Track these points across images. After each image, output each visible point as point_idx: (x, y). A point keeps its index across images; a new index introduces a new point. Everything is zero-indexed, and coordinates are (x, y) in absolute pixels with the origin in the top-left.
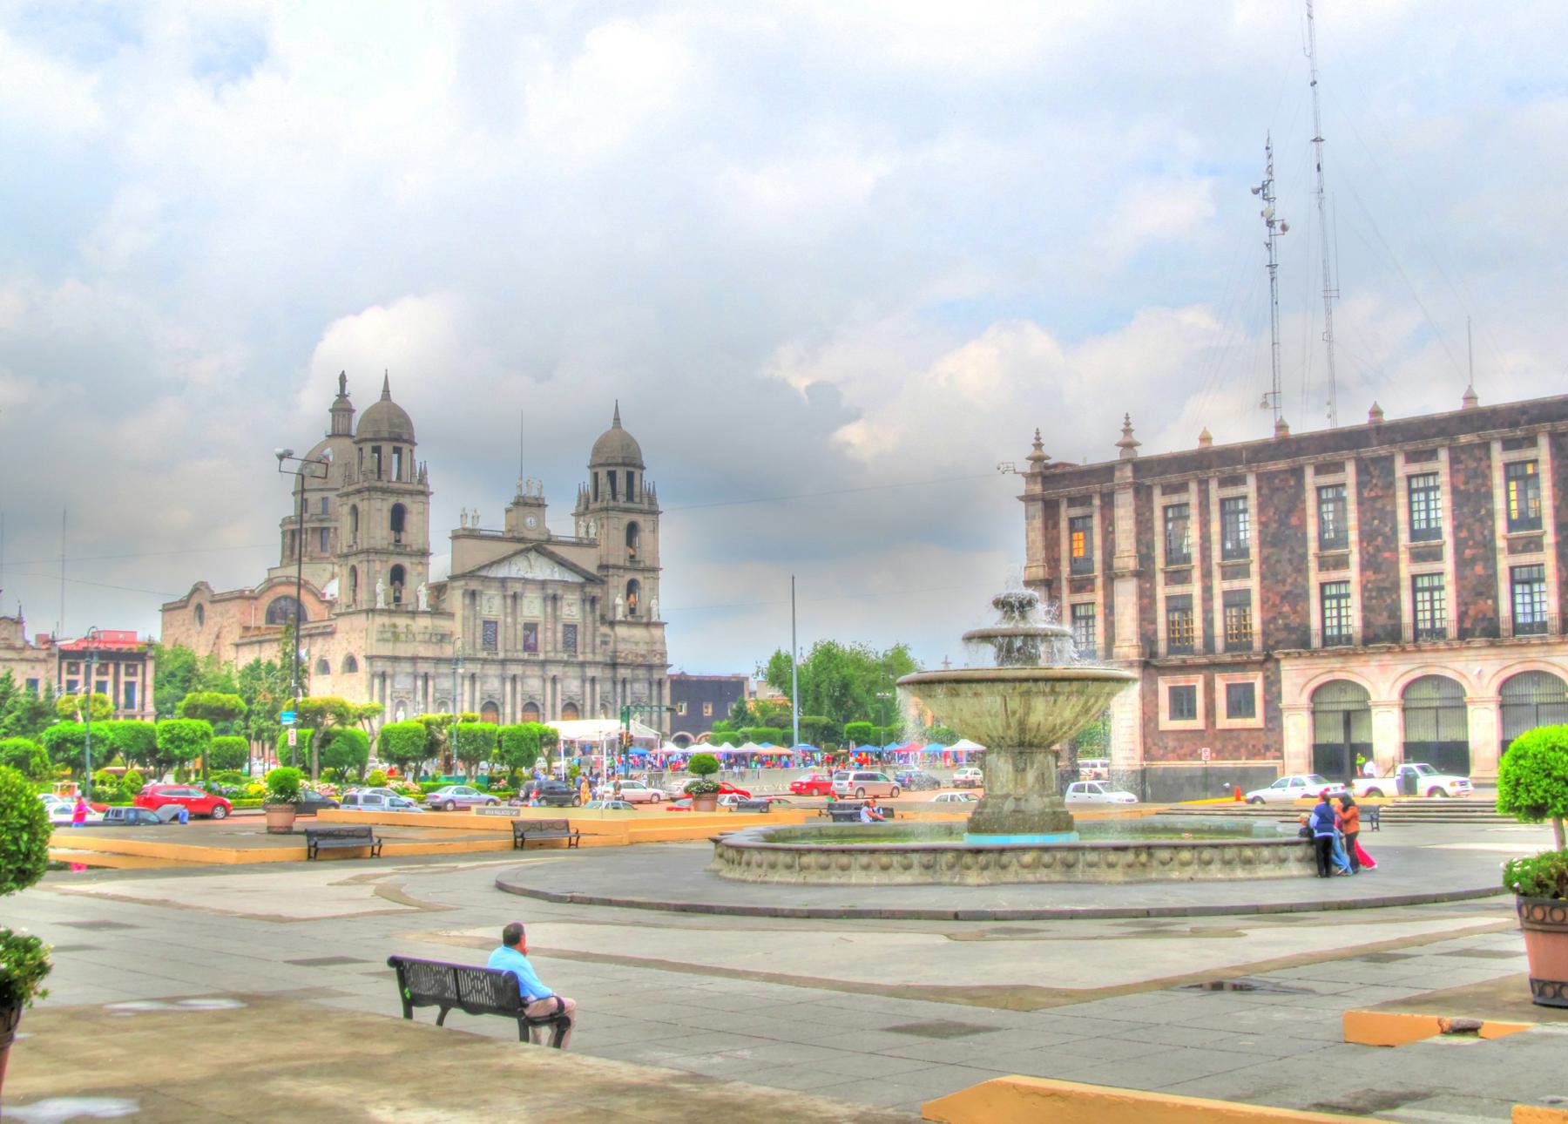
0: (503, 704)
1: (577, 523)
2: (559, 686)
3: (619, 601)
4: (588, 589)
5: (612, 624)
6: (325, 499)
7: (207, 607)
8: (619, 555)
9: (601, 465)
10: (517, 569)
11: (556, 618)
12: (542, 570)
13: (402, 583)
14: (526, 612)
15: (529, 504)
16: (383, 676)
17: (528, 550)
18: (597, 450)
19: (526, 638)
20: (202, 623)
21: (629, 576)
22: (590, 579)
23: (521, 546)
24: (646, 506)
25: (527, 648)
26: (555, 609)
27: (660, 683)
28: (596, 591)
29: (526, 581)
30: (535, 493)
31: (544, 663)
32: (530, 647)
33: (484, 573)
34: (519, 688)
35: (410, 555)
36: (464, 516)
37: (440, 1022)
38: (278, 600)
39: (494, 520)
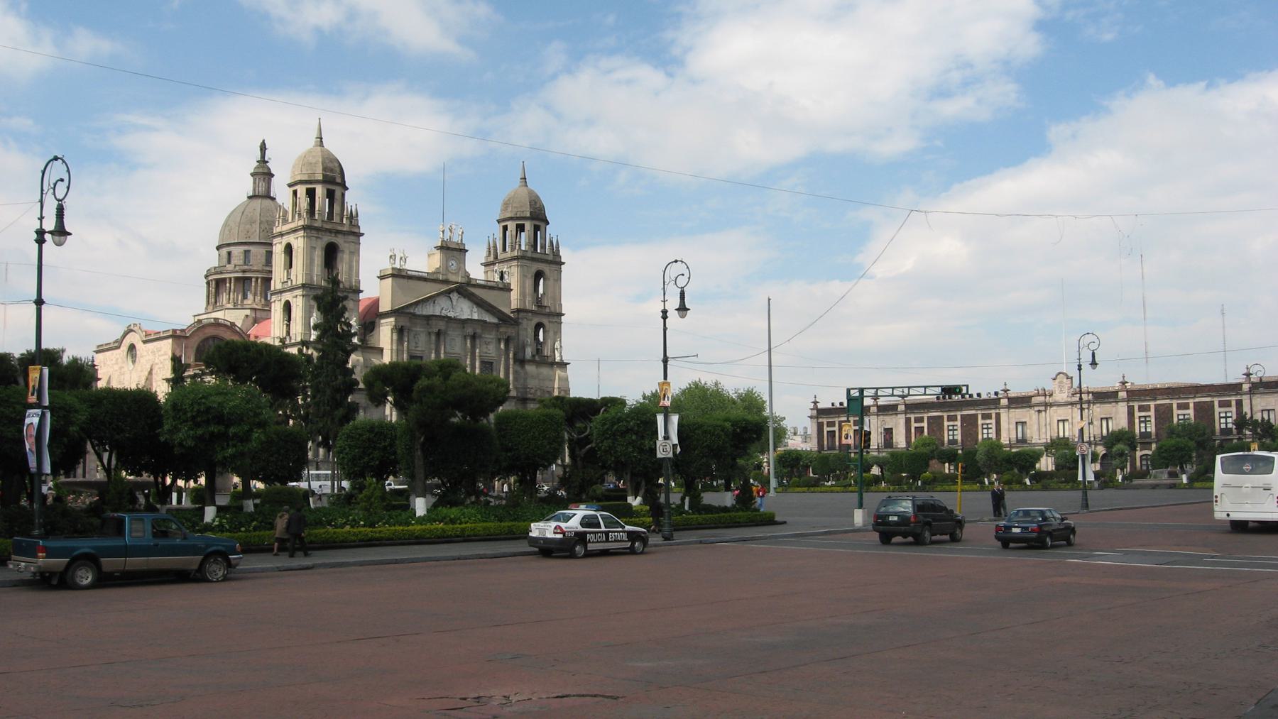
4: (502, 330)
6: (247, 252)
7: (140, 346)
12: (465, 310)
15: (454, 251)
17: (448, 293)
18: (506, 205)
20: (134, 362)
21: (536, 320)
22: (504, 319)
23: (444, 288)
24: (551, 258)
28: (510, 331)
30: (456, 239)
36: (393, 257)
38: (207, 339)
39: (424, 261)
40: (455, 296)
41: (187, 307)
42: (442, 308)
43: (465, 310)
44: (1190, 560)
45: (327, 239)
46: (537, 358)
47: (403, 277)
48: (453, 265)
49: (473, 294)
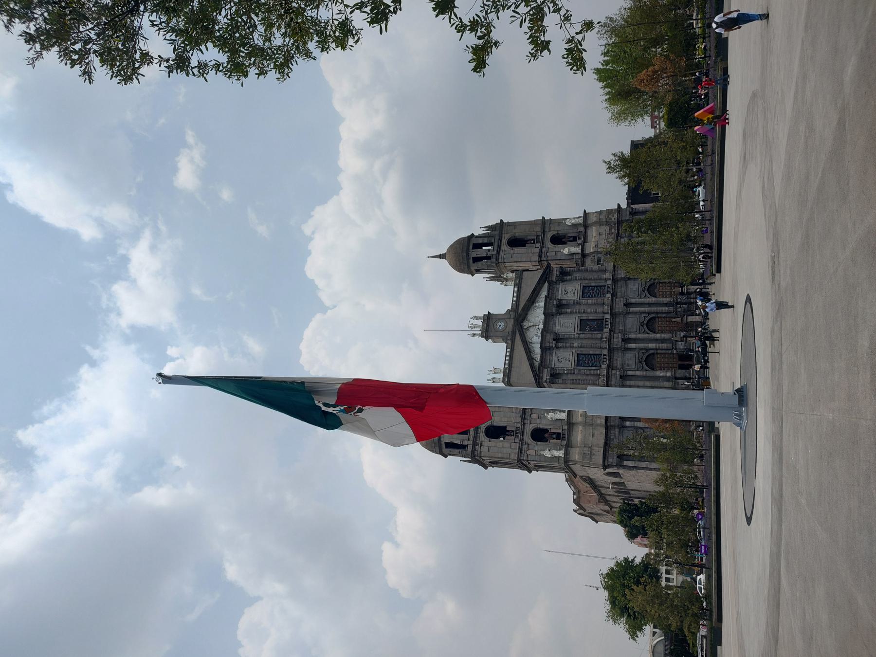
0: (647, 350)
1: (480, 318)
2: (633, 301)
3: (566, 251)
5: (584, 255)
8: (531, 251)
9: (469, 267)
10: (535, 338)
11: (577, 303)
12: (537, 316)
13: (546, 431)
14: (571, 330)
16: (621, 457)
18: (461, 271)
19: (592, 329)
21: (548, 244)
22: (545, 277)
24: (497, 233)
25: (600, 329)
26: (567, 305)
27: (634, 213)
29: (544, 331)
30: (479, 322)
31: (613, 315)
32: (599, 325)
33: (537, 364)
34: (633, 336)
35: (524, 425)
37: (397, 545)
40: (526, 324)
41: (589, 91)
42: (535, 338)
43: (537, 316)
44: (702, 648)
45: (505, 247)
46: (580, 242)
47: (510, 371)
48: (501, 325)
49: (523, 309)
